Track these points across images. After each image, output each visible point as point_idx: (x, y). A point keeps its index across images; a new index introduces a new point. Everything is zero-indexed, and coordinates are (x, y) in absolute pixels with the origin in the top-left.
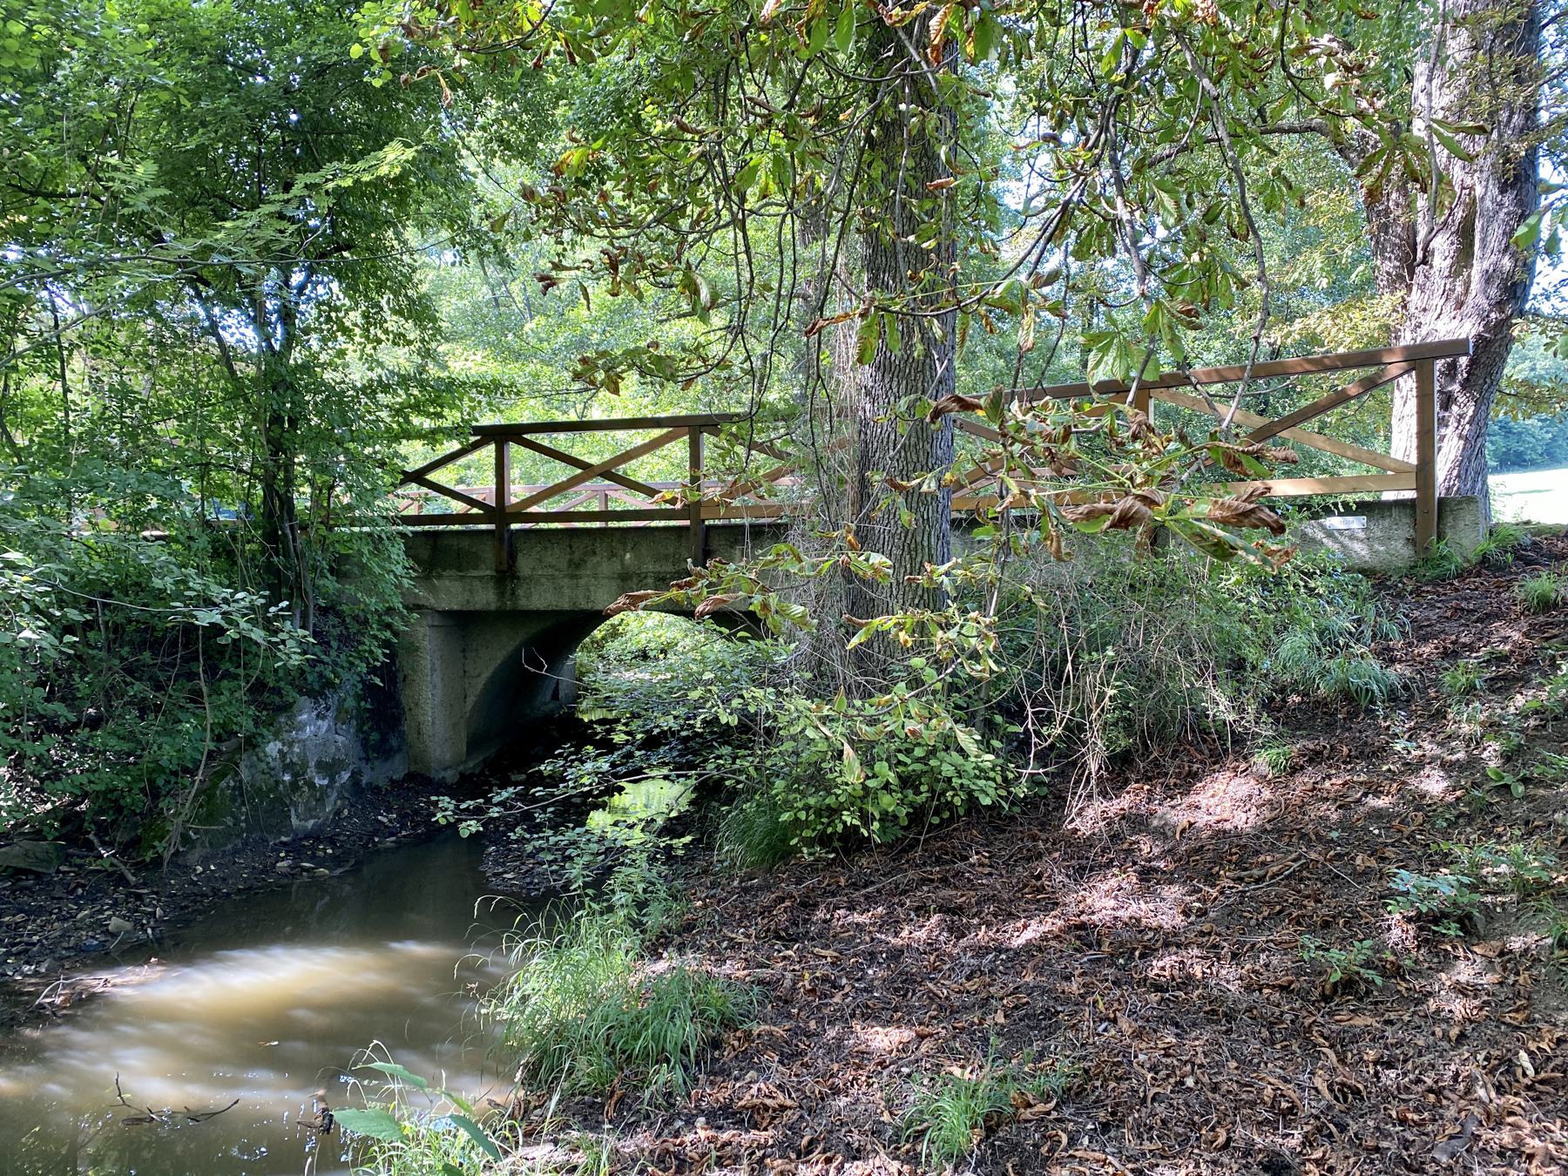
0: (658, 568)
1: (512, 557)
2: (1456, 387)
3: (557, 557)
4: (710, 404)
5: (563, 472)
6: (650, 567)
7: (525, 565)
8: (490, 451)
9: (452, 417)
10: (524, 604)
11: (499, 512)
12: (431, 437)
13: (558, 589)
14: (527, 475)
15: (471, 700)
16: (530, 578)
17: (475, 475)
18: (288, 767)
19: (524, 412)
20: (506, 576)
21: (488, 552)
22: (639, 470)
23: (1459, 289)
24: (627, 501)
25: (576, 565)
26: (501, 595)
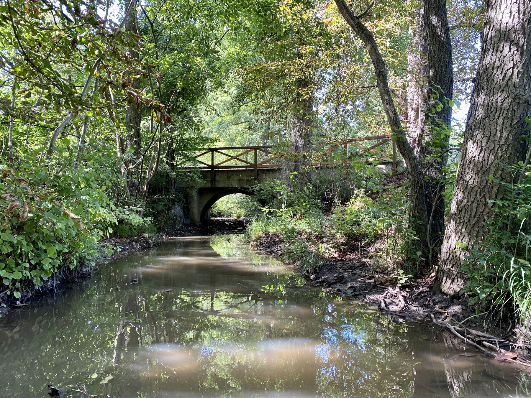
0: (247, 178)
1: (215, 176)
2: (416, 145)
3: (225, 176)
4: (402, 212)
5: (241, 158)
6: (245, 178)
7: (217, 178)
8: (210, 153)
9: (206, 146)
10: (217, 186)
11: (212, 167)
12: (200, 150)
13: (225, 183)
14: (219, 158)
15: (201, 209)
16: (218, 181)
17: (206, 159)
18: (175, 215)
19: (217, 145)
20: (213, 180)
21: (209, 175)
22: (225, 158)
23: (416, 123)
24: (240, 163)
25: (229, 178)
26: (212, 184)
